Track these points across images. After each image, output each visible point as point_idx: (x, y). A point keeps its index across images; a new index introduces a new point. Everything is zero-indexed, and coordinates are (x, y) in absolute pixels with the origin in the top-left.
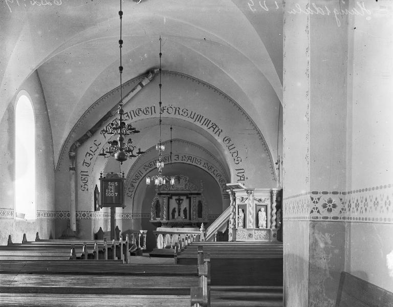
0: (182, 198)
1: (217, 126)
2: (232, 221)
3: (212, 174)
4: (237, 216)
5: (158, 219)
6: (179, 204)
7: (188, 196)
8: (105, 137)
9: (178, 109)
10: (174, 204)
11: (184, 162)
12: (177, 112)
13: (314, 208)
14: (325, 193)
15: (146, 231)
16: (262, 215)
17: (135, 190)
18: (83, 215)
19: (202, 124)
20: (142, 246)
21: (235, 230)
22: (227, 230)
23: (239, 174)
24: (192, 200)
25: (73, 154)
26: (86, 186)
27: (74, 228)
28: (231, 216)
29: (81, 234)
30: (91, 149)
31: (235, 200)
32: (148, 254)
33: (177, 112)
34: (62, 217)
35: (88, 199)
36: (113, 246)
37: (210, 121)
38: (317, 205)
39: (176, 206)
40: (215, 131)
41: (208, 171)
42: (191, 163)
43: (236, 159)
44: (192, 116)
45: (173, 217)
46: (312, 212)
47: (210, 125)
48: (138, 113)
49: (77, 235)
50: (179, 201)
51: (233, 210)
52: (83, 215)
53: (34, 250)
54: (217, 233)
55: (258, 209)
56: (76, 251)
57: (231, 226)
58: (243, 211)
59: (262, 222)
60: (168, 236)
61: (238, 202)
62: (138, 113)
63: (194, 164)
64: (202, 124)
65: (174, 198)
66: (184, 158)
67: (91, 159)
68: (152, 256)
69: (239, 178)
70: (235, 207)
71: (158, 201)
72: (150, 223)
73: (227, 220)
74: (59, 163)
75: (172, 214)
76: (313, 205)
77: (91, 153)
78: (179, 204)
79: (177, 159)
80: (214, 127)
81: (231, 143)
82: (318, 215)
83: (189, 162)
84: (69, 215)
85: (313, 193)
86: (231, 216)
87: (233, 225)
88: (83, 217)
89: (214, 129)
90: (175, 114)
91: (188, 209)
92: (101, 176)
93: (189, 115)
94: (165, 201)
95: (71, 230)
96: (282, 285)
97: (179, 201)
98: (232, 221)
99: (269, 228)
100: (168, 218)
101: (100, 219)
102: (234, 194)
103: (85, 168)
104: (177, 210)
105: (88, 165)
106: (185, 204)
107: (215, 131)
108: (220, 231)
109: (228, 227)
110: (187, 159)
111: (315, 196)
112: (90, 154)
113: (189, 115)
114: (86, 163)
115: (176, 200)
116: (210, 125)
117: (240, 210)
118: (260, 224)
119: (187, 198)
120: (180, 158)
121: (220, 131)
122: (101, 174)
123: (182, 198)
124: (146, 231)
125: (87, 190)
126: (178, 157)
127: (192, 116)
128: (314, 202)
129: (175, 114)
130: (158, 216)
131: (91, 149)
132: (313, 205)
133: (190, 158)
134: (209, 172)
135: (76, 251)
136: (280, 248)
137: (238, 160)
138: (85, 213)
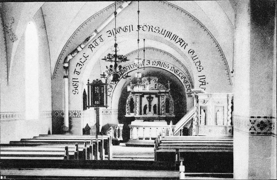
0: (152, 96)
1: (183, 41)
2: (196, 119)
3: (178, 76)
4: (199, 115)
5: (132, 115)
6: (150, 102)
7: (158, 95)
8: (92, 51)
9: (151, 27)
10: (145, 101)
11: (154, 66)
12: (151, 29)
13: (252, 127)
14: (259, 117)
15: (122, 125)
16: (220, 115)
17: (113, 90)
18: (74, 114)
19: (171, 39)
20: (119, 137)
21: (198, 125)
22: (192, 126)
23: (201, 80)
24: (161, 98)
25: (66, 65)
26: (76, 90)
27: (67, 124)
28: (195, 115)
29: (73, 129)
30: (81, 60)
31: (198, 102)
32: (124, 144)
33: (151, 29)
34: (58, 116)
35: (77, 102)
36: (102, 141)
37: (178, 37)
38: (254, 125)
39: (147, 103)
40: (182, 44)
41: (174, 74)
42: (160, 67)
43: (199, 68)
44: (163, 33)
45: (145, 113)
46: (250, 129)
47: (178, 40)
48: (118, 31)
49: (70, 131)
50: (150, 99)
51: (196, 111)
52: (74, 114)
53: (40, 145)
54: (183, 128)
55: (217, 110)
56: (79, 146)
57: (195, 123)
58: (204, 111)
59: (220, 121)
60: (141, 129)
61: (200, 104)
62: (118, 31)
63: (162, 68)
64: (171, 39)
65: (146, 96)
66: (154, 63)
67: (80, 69)
68: (127, 145)
69: (201, 83)
70: (198, 108)
71: (132, 99)
72: (125, 117)
73: (191, 118)
74: (55, 72)
75: (144, 110)
76: (251, 125)
77: (80, 63)
78: (150, 102)
79: (148, 64)
80: (181, 41)
81: (195, 54)
82: (254, 131)
83: (158, 66)
84: (63, 114)
85: (252, 117)
86: (195, 115)
87: (196, 122)
88: (74, 116)
89: (181, 43)
90: (149, 31)
91: (157, 106)
92: (88, 82)
93: (160, 32)
94: (138, 99)
95: (65, 127)
96: (232, 172)
97: (150, 99)
98: (196, 119)
99: (225, 125)
100: (141, 114)
101: (88, 117)
102: (197, 97)
103: (76, 76)
104: (148, 106)
105: (78, 73)
106: (155, 101)
107: (182, 44)
108: (185, 127)
109: (192, 124)
110: (157, 64)
111: (252, 119)
112: (80, 65)
113: (160, 32)
114: (76, 71)
115: (147, 98)
116: (178, 40)
117: (202, 110)
118: (204, 78)
119: (156, 96)
120: (151, 63)
121: (186, 44)
122: (88, 80)
123: (152, 96)
124: (122, 125)
125: (78, 93)
126: (149, 63)
127: (163, 33)
128: (252, 123)
129: (149, 31)
130: (132, 111)
131: (81, 60)
132: (251, 125)
133: (159, 63)
134: (176, 75)
135: (79, 146)
136: (230, 146)
137: (200, 69)
138: (76, 112)
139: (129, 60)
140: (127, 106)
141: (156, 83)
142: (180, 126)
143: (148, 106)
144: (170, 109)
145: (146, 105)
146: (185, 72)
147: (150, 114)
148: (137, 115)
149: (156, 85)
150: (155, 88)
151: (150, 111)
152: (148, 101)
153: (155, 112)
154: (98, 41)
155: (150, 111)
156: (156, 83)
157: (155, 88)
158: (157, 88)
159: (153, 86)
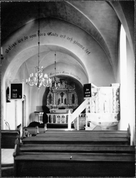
71: (50, 95)
139: (129, 124)
140: (48, 99)
141: (66, 85)
142: (34, 155)
143: (61, 100)
144: (75, 101)
145: (60, 99)
146: (19, 28)
147: (62, 105)
148: (55, 105)
149: (66, 86)
150: (66, 87)
151: (62, 102)
152: (61, 96)
153: (65, 103)
154: (63, 37)
155: (62, 102)
156: (66, 85)
157: (66, 87)
158: (66, 88)
159: (64, 87)
